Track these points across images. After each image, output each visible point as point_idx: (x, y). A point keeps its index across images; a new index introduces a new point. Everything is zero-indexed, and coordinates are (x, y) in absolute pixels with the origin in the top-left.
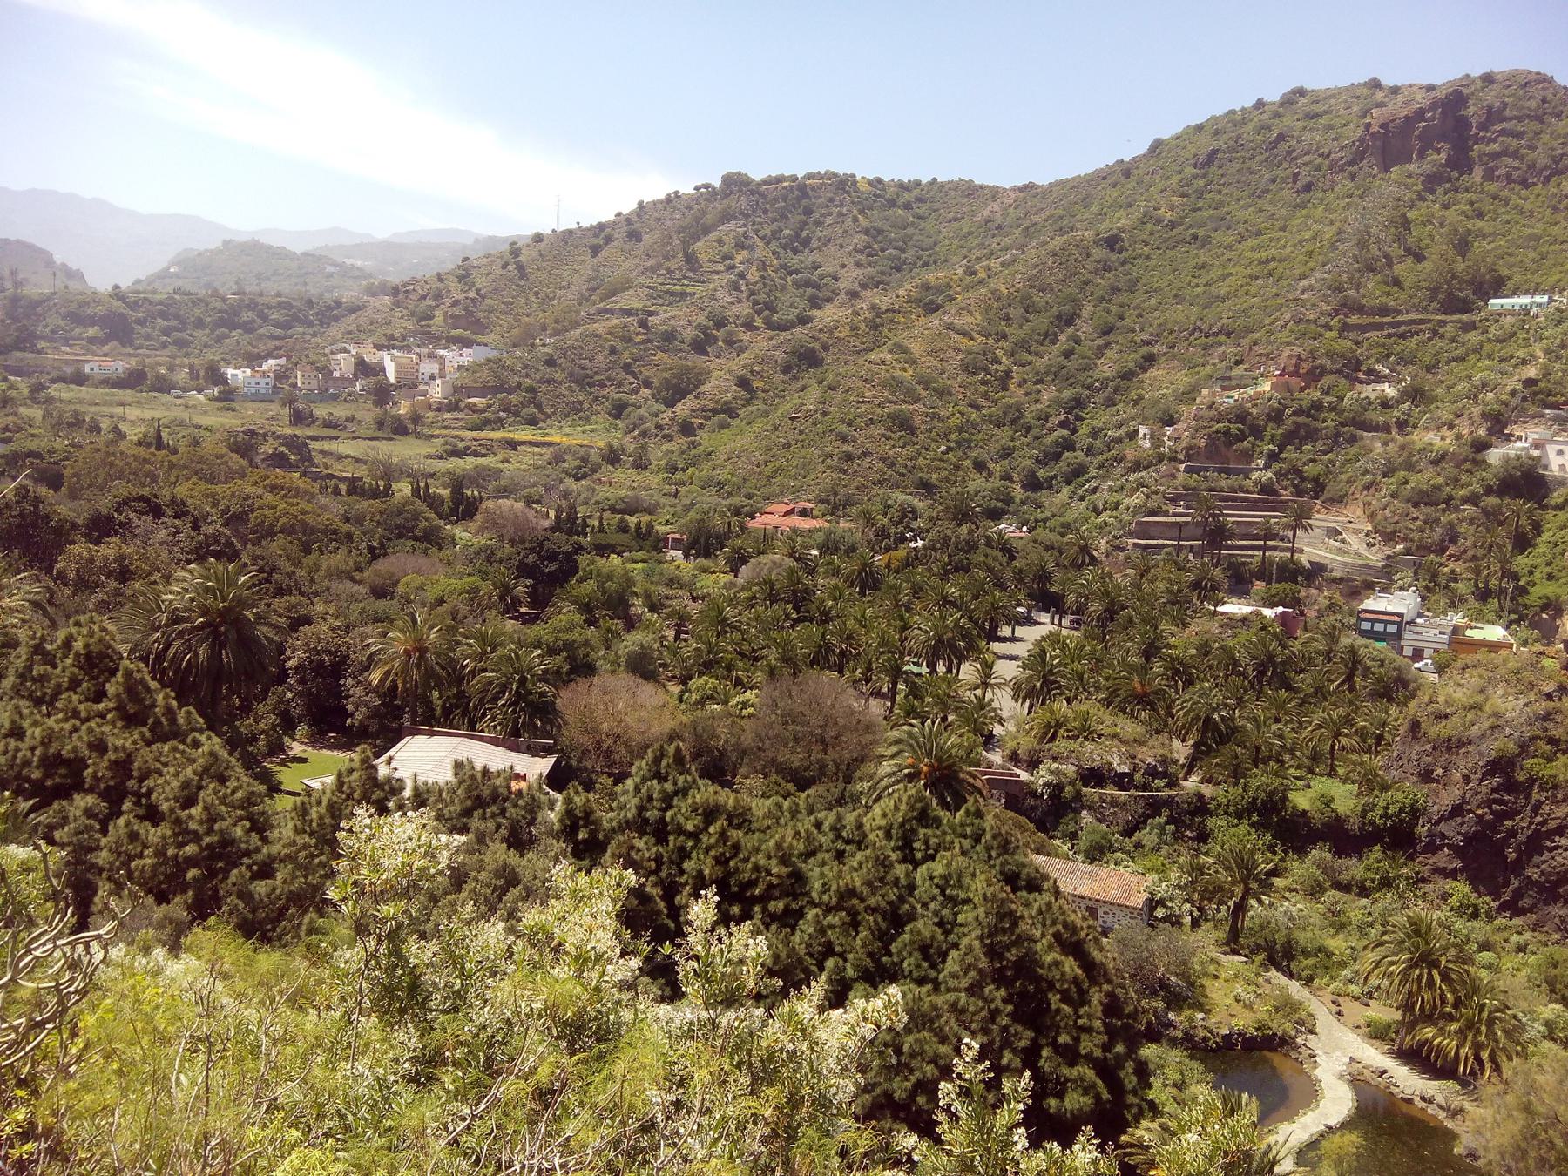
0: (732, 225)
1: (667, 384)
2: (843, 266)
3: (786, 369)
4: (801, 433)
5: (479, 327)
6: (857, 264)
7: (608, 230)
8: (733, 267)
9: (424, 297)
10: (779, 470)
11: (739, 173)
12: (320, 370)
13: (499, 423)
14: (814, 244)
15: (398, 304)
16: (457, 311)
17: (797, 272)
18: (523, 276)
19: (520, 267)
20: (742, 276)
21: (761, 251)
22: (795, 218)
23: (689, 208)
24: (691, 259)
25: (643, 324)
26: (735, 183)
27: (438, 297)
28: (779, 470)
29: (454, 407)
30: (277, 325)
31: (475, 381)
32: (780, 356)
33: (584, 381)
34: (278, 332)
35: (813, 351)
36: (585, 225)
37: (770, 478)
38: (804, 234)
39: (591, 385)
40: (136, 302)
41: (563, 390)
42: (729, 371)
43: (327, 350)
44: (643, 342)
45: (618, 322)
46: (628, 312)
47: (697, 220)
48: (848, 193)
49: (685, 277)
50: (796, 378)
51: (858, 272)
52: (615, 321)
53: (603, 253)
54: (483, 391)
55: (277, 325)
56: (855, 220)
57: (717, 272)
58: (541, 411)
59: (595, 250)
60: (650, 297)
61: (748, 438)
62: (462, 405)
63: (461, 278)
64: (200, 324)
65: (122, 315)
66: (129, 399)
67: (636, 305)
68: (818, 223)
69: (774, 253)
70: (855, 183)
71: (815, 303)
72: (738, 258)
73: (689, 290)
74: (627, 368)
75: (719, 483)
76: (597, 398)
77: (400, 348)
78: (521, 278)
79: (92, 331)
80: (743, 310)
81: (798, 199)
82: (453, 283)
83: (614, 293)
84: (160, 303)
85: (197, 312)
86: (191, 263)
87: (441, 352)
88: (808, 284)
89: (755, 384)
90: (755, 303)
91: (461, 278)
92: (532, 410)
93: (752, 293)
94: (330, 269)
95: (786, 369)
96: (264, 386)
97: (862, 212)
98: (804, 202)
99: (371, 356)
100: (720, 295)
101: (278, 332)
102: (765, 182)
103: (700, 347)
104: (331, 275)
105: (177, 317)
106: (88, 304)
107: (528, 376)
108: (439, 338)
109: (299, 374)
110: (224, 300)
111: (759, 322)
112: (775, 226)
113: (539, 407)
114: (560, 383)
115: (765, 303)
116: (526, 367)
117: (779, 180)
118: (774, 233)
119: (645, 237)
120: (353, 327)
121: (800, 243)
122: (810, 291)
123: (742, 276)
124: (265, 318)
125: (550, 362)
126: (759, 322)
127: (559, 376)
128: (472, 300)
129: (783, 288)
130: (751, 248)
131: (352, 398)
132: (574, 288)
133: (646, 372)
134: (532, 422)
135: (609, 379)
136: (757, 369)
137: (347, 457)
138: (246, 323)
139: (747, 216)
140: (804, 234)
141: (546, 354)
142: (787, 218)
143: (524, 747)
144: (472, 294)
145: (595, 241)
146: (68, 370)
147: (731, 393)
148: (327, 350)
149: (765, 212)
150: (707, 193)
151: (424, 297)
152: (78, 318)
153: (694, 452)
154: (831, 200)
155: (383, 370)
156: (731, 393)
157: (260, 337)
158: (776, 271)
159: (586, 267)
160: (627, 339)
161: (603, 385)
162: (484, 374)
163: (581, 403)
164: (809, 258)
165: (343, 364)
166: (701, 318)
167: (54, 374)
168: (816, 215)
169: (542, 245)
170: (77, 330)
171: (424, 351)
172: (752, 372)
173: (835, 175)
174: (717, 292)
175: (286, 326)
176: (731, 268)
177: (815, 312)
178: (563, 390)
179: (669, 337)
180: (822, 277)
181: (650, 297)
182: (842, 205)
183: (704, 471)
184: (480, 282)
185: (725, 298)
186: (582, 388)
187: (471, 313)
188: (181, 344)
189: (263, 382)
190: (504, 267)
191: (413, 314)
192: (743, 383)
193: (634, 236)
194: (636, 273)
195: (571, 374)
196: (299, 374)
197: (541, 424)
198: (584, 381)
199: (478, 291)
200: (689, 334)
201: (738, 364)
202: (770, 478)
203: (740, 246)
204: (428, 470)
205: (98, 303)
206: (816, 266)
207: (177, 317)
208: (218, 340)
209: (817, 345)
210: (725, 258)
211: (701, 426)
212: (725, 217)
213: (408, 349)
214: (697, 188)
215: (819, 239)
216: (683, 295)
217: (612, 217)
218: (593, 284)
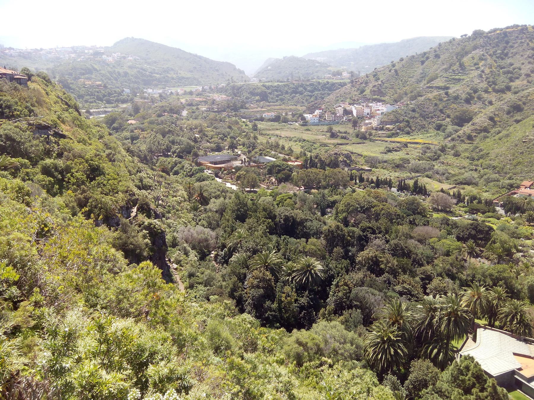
0: (477, 51)
1: (457, 117)
2: (523, 64)
3: (508, 113)
4: (528, 148)
5: (383, 94)
6: (529, 63)
7: (427, 55)
8: (479, 68)
9: (362, 83)
10: (519, 163)
11: (480, 30)
12: (333, 113)
13: (396, 135)
14: (510, 55)
15: (353, 86)
16: (375, 89)
17: (504, 68)
18: (397, 74)
19: (396, 71)
20: (483, 71)
21: (490, 61)
22: (502, 46)
23: (459, 44)
24: (462, 66)
25: (447, 94)
26: (478, 34)
27: (366, 83)
28: (519, 163)
29: (382, 129)
30: (310, 91)
31: (388, 119)
32: (506, 108)
33: (424, 117)
34: (310, 94)
35: (519, 105)
36: (419, 53)
37: (515, 166)
38: (505, 52)
39: (428, 118)
40: (268, 87)
41: (418, 120)
42: (485, 114)
43: (335, 107)
44: (447, 100)
45: (437, 93)
46: (439, 88)
47: (463, 49)
48: (524, 33)
49: (460, 73)
50: (512, 116)
51: (530, 66)
52: (435, 93)
53: (426, 63)
54: (391, 123)
55: (310, 91)
56: (528, 44)
57: (472, 70)
58: (411, 129)
59: (423, 63)
60: (446, 81)
61: (504, 149)
62: (385, 128)
63: (374, 76)
64: (287, 93)
65: (265, 92)
66: (278, 127)
67: (441, 84)
68: (512, 47)
69: (495, 61)
70: (527, 29)
71: (511, 80)
72: (481, 64)
73: (462, 78)
74: (441, 111)
75: (494, 167)
76: (430, 123)
77: (357, 104)
78: (396, 75)
79: (257, 98)
80: (484, 85)
81: (504, 38)
82: (371, 78)
83: (432, 80)
84: (275, 87)
85: (286, 89)
86: (276, 65)
87: (370, 104)
88: (509, 72)
89: (496, 119)
90: (489, 82)
91: (374, 76)
92: (408, 129)
93: (487, 78)
94: (317, 64)
95: (508, 113)
96: (316, 120)
97: (530, 41)
98: (506, 39)
99: (348, 108)
100: (474, 80)
101: (310, 94)
102: (490, 32)
103: (468, 101)
104: (317, 67)
105: (280, 91)
106: (255, 89)
107: (406, 116)
108: (369, 99)
109: (326, 115)
110: (294, 84)
111: (490, 90)
112: (494, 50)
113: (410, 127)
114: (417, 118)
115: (492, 82)
116: (405, 113)
117: (495, 30)
118: (494, 52)
119: (441, 56)
120: (339, 95)
121: (504, 55)
122: (510, 75)
123: (483, 71)
124: (305, 89)
125: (414, 111)
126: (490, 90)
127: (417, 115)
128: (380, 85)
129: (499, 75)
130: (486, 60)
131: (343, 123)
132: (415, 77)
133: (448, 112)
134: (408, 133)
135: (435, 115)
136: (497, 113)
137: (355, 153)
138: (300, 91)
139: (483, 47)
140: (505, 52)
141: (412, 108)
142: (499, 46)
143: (522, 339)
144: (380, 83)
145: (422, 59)
146: (259, 116)
147: (487, 123)
148: (335, 107)
149: (490, 44)
150: (465, 39)
151: (362, 83)
152: (253, 94)
153: (481, 153)
154: (517, 37)
155: (352, 112)
156: (487, 123)
157: (305, 96)
158: (496, 68)
159: (419, 69)
160: (441, 100)
161: (432, 118)
162: (392, 117)
163: (425, 125)
164: (509, 61)
165: (340, 111)
166: (468, 90)
167: (255, 118)
168: (510, 44)
169: (404, 62)
170: (253, 97)
171: (364, 104)
172: (495, 114)
173: (518, 26)
174: (472, 76)
175: (312, 91)
176: (477, 68)
177: (512, 84)
178: (418, 120)
179: (456, 98)
180: (514, 69)
181: (446, 81)
182: (522, 39)
183: (485, 162)
184: (382, 78)
185: (477, 81)
186: (425, 119)
187: (379, 90)
188: (282, 100)
189: (316, 119)
190: (390, 71)
191: (358, 89)
192: (491, 119)
193: (437, 56)
194: (439, 71)
195: (421, 115)
196: (326, 115)
197: (411, 134)
198: (424, 117)
199: (382, 81)
200: (464, 96)
201: (490, 110)
202: (515, 166)
203: (481, 59)
204: (385, 159)
205: (259, 88)
206: (512, 65)
207: (280, 91)
208: (292, 98)
209: (520, 103)
210: (475, 64)
211: (475, 136)
212: (475, 48)
213: (359, 104)
214: (462, 36)
215: (512, 53)
216: (459, 80)
217: (429, 50)
218: (422, 75)
